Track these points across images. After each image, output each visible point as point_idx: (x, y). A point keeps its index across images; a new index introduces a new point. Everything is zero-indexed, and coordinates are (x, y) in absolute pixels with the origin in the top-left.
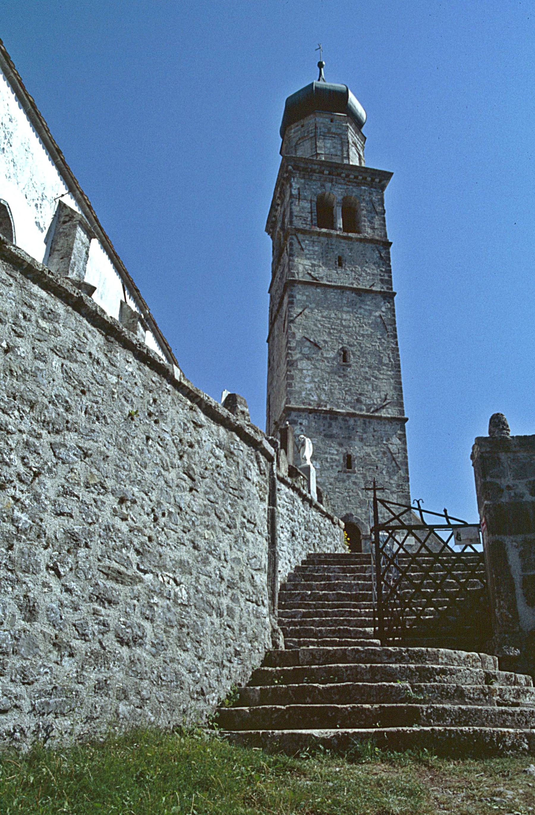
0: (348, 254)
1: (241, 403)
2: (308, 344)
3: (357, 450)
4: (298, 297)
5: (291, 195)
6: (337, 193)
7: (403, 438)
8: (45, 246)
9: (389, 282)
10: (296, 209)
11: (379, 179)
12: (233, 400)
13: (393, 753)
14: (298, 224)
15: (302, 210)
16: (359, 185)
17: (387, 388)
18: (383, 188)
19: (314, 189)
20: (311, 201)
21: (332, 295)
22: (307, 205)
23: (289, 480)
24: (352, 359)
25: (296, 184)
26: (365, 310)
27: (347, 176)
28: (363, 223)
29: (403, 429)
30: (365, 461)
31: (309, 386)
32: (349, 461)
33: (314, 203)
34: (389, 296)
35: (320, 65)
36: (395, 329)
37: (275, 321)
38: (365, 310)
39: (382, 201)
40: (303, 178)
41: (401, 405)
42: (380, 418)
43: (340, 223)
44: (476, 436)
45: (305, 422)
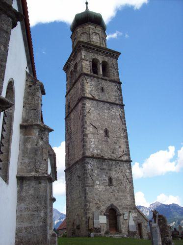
2: (92, 126)
3: (114, 174)
4: (87, 104)
5: (82, 59)
6: (100, 58)
10: (84, 64)
12: (162, 219)
14: (85, 71)
15: (86, 66)
17: (123, 147)
18: (117, 59)
20: (90, 62)
21: (101, 104)
22: (88, 63)
23: (104, 78)
26: (114, 112)
27: (104, 52)
28: (110, 69)
30: (118, 179)
31: (93, 146)
32: (110, 180)
33: (91, 62)
34: (122, 106)
36: (125, 121)
38: (114, 112)
40: (86, 51)
41: (129, 155)
44: (138, 167)
45: (92, 163)
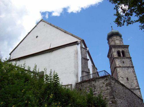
0: (124, 61)
1: (78, 80)
5: (113, 52)
6: (121, 50)
7: (140, 92)
8: (108, 59)
9: (132, 65)
11: (127, 47)
13: (50, 81)
14: (115, 57)
15: (115, 54)
16: (124, 48)
17: (136, 83)
18: (128, 48)
19: (117, 50)
24: (129, 79)
25: (113, 50)
29: (140, 90)
34: (133, 67)
35: (112, 27)
37: (113, 73)
39: (128, 50)
42: (135, 89)
43: (122, 56)
